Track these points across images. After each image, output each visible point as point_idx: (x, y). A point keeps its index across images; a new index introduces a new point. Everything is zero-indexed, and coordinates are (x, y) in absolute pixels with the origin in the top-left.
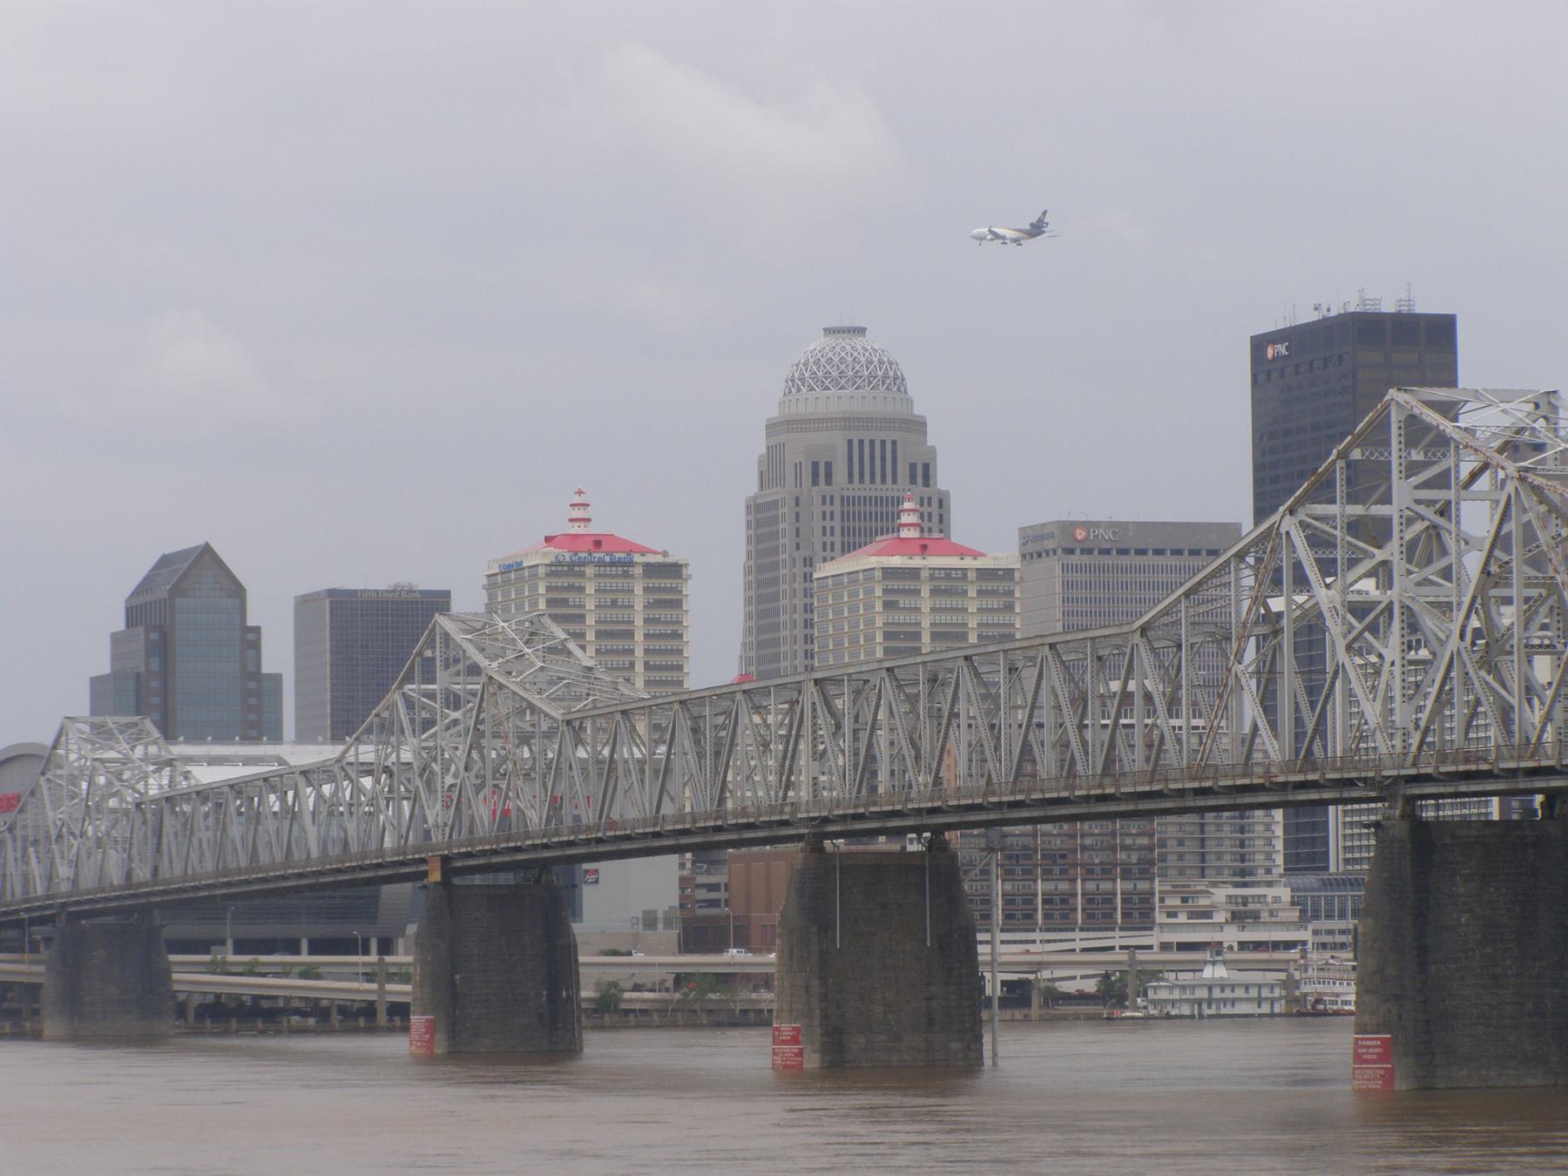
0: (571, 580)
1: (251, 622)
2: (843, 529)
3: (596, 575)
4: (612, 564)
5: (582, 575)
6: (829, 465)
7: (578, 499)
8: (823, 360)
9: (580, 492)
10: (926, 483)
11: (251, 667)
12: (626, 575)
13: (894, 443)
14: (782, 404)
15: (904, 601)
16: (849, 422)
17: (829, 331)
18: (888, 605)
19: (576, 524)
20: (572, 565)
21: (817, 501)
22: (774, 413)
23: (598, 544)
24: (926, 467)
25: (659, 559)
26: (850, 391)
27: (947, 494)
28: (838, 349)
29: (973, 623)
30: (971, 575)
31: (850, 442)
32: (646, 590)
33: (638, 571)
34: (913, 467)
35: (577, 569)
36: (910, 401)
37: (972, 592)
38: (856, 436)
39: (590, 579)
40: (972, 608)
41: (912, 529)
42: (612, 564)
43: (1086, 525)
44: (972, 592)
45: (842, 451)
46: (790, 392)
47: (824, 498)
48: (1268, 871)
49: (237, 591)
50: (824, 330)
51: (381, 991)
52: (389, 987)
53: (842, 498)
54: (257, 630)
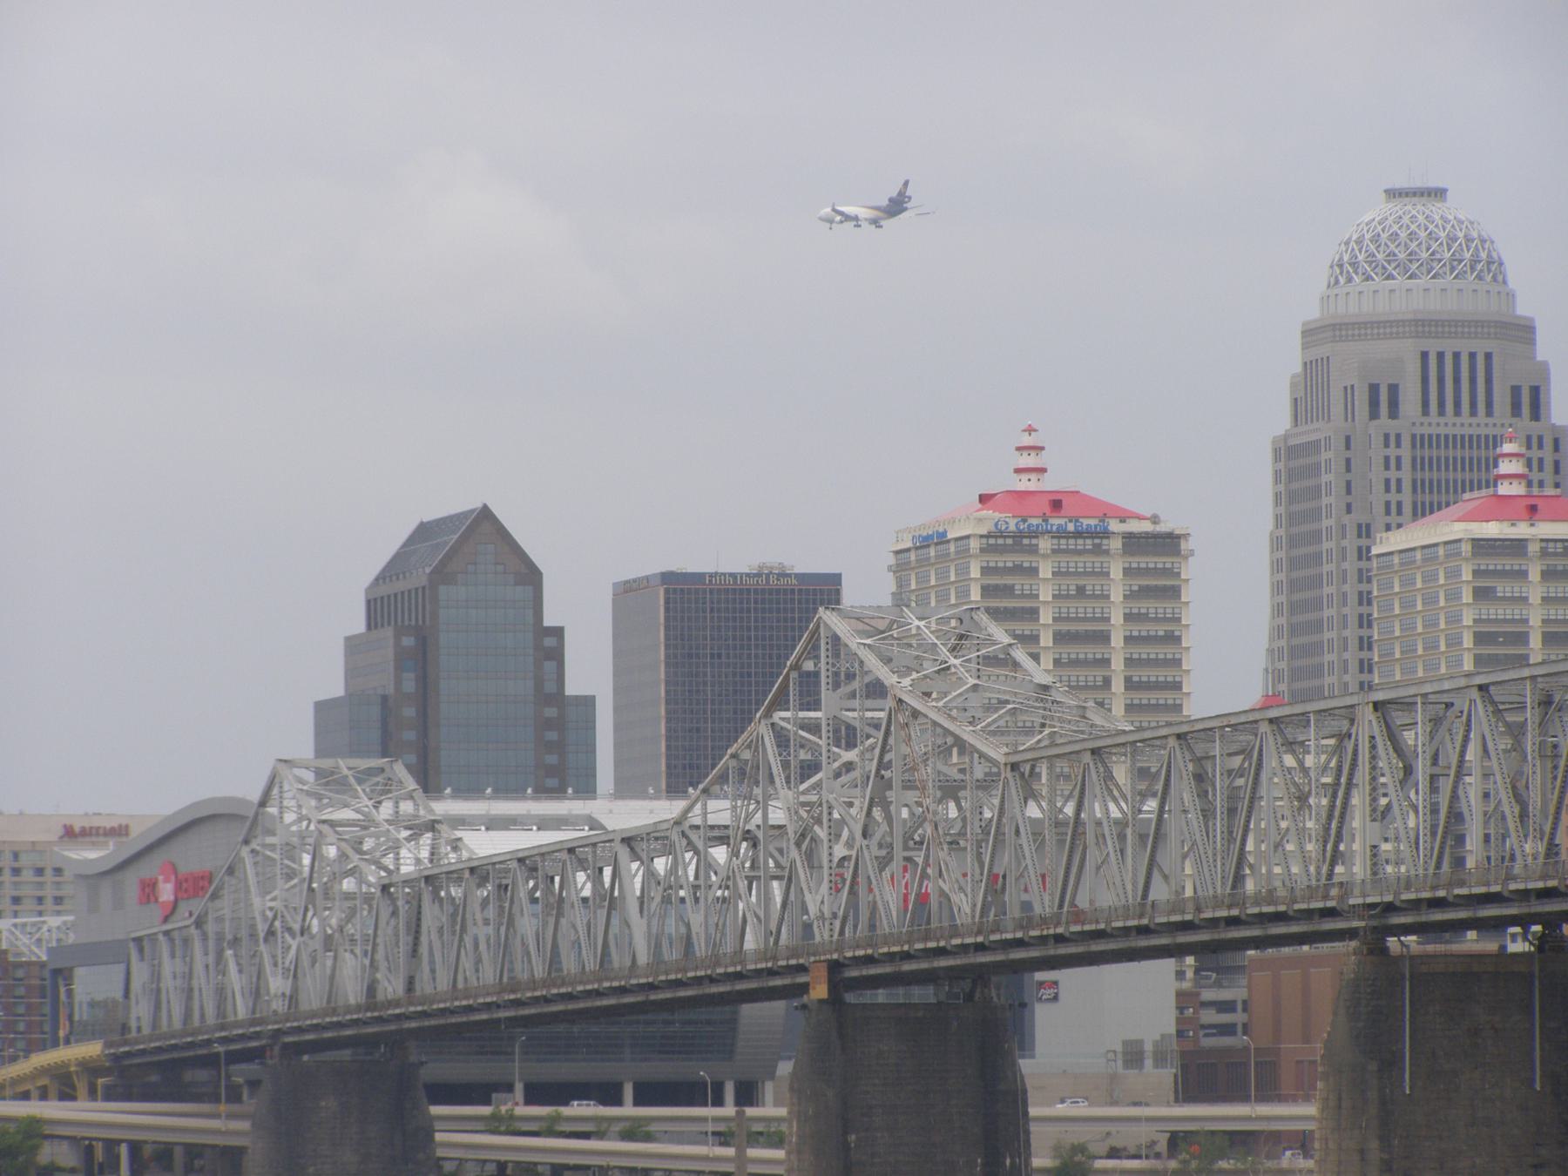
0: (1018, 558)
1: (549, 620)
3: (982, 550)
4: (1078, 534)
5: (1033, 550)
6: (1393, 389)
7: (1027, 440)
8: (1384, 236)
9: (1030, 430)
10: (1536, 415)
11: (550, 687)
12: (1098, 551)
13: (1488, 356)
14: (1325, 299)
15: (1503, 588)
16: (1423, 326)
17: (1393, 194)
18: (1481, 594)
19: (1024, 477)
20: (1018, 536)
22: (1312, 312)
23: (1056, 505)
24: (1535, 392)
26: (1423, 281)
28: (1406, 220)
32: (1128, 572)
33: (1116, 544)
34: (1516, 391)
35: (1026, 541)
36: (1511, 296)
38: (1433, 346)
39: (1045, 556)
41: (1515, 482)
42: (1078, 534)
45: (1413, 368)
46: (1337, 282)
47: (1387, 436)
49: (531, 576)
51: (741, 1159)
52: (753, 1153)
53: (1414, 437)
54: (558, 632)
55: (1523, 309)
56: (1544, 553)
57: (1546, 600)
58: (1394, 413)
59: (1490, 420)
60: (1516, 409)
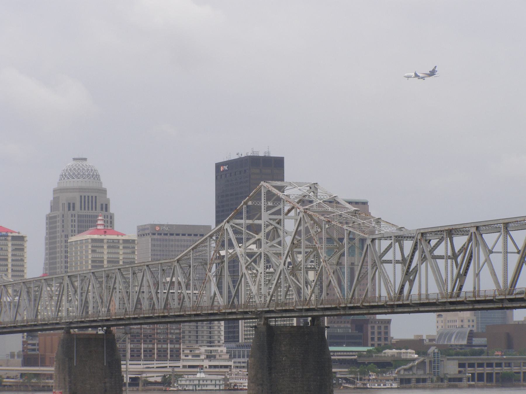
2: (78, 225)
6: (74, 204)
12: (6, 240)
14: (58, 183)
15: (98, 250)
16: (81, 190)
17: (75, 159)
21: (70, 216)
22: (56, 186)
24: (106, 205)
25: (17, 234)
26: (81, 179)
27: (113, 214)
29: (121, 257)
30: (121, 242)
31: (81, 196)
32: (12, 245)
33: (10, 238)
34: (102, 205)
36: (101, 183)
37: (121, 247)
38: (83, 194)
40: (121, 252)
41: (101, 226)
43: (160, 225)
44: (121, 247)
45: (78, 199)
47: (72, 215)
48: (219, 342)
50: (73, 159)
53: (78, 215)
55: (103, 187)
56: (108, 242)
57: (108, 253)
58: (74, 210)
59: (96, 212)
60: (102, 209)
